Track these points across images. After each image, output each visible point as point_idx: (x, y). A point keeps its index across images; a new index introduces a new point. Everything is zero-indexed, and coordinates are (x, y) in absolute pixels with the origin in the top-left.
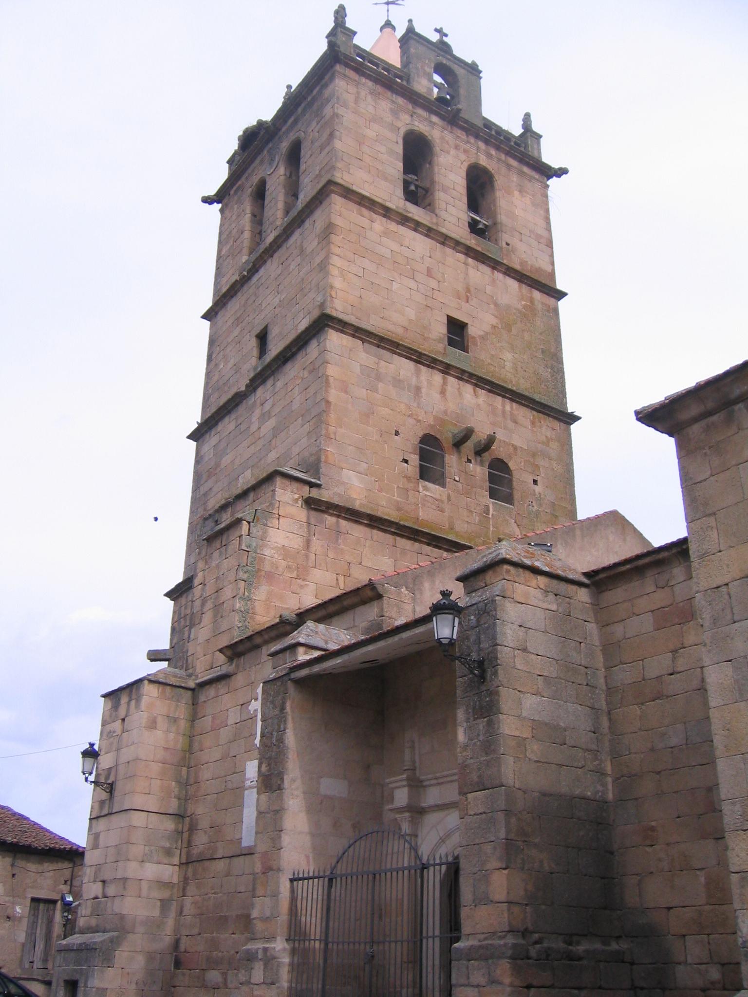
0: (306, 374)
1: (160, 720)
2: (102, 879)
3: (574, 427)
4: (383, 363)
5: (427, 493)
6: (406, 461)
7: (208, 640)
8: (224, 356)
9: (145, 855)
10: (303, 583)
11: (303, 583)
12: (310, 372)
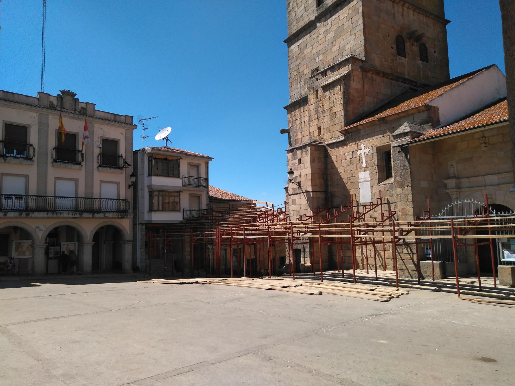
1: (316, 159)
3: (448, 26)
4: (382, 4)
6: (392, 48)
7: (329, 127)
8: (297, 4)
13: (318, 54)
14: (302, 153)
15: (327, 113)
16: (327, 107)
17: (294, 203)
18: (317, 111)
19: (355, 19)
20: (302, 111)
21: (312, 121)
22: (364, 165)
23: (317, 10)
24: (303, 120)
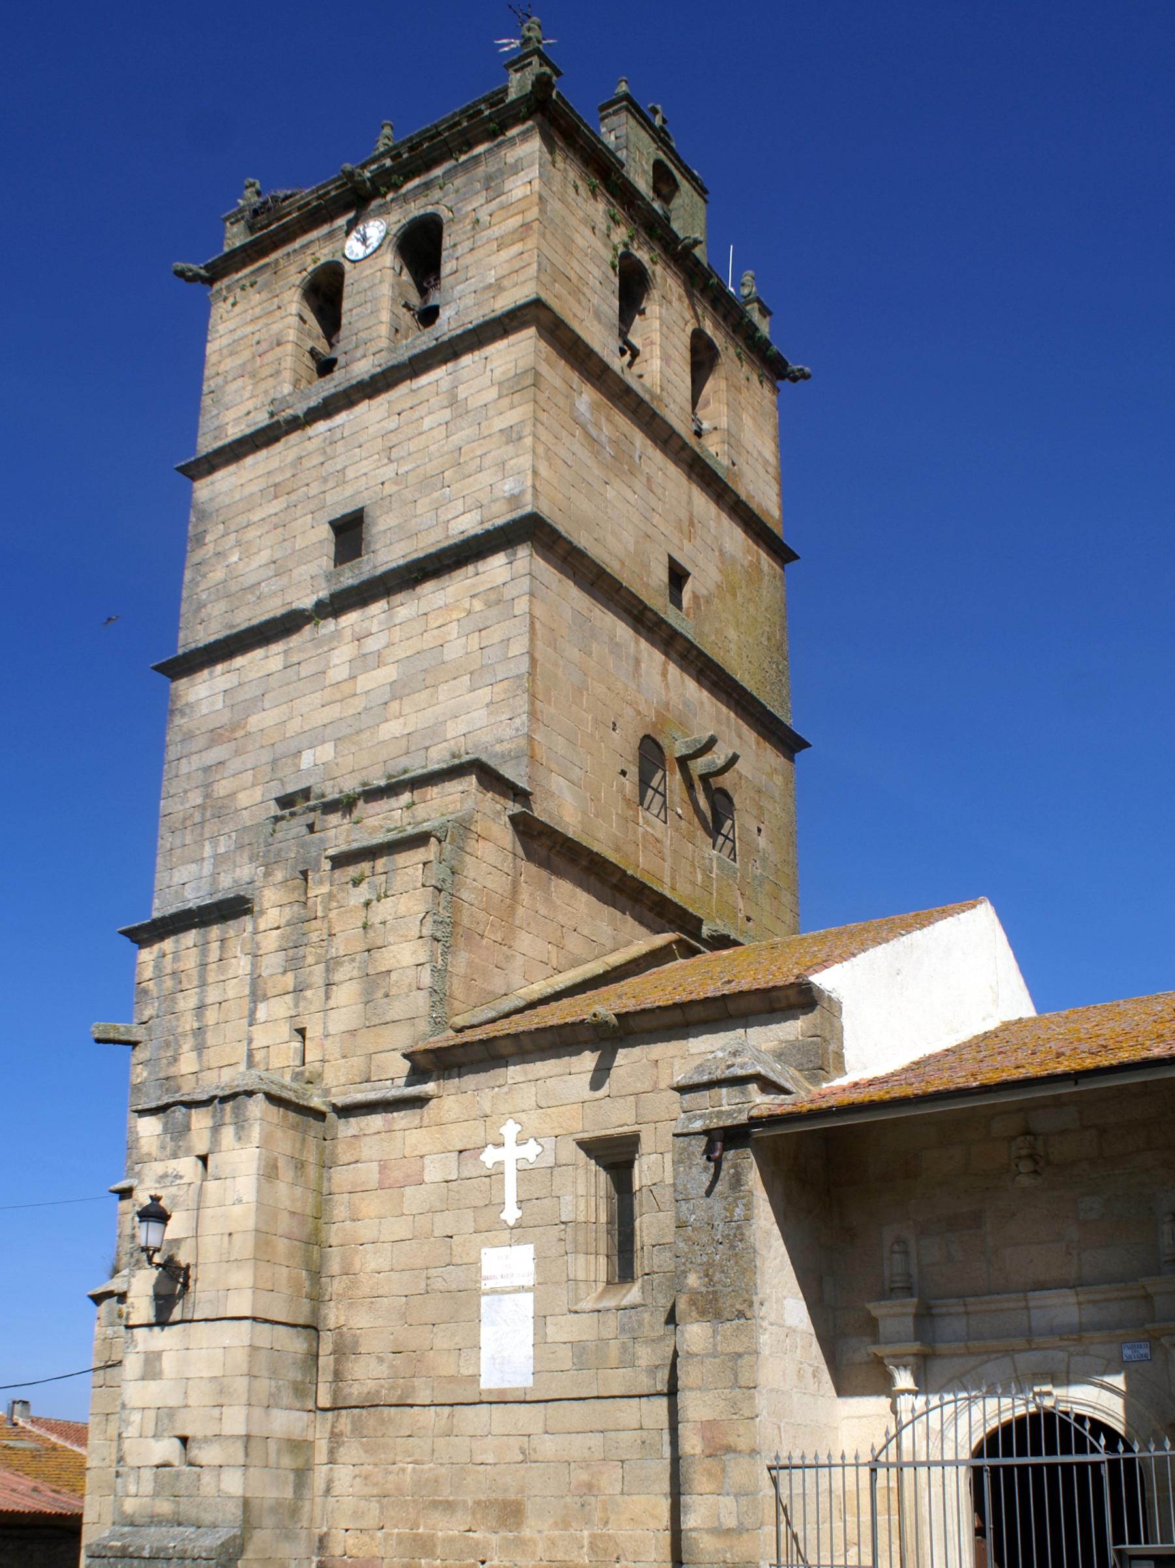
0: (478, 605)
1: (281, 1164)
2: (180, 1433)
5: (649, 829)
6: (624, 773)
7: (352, 1032)
9: (271, 1395)
10: (509, 952)
11: (509, 952)
12: (488, 605)
13: (315, 738)
14: (216, 1129)
15: (345, 972)
16: (347, 939)
17: (151, 1368)
18: (294, 964)
19: (495, 635)
20: (214, 955)
21: (265, 998)
22: (511, 1214)
23: (329, 577)
24: (212, 996)
